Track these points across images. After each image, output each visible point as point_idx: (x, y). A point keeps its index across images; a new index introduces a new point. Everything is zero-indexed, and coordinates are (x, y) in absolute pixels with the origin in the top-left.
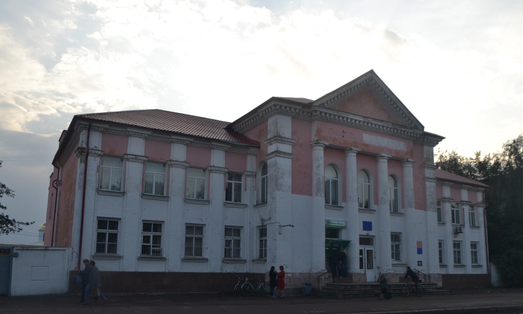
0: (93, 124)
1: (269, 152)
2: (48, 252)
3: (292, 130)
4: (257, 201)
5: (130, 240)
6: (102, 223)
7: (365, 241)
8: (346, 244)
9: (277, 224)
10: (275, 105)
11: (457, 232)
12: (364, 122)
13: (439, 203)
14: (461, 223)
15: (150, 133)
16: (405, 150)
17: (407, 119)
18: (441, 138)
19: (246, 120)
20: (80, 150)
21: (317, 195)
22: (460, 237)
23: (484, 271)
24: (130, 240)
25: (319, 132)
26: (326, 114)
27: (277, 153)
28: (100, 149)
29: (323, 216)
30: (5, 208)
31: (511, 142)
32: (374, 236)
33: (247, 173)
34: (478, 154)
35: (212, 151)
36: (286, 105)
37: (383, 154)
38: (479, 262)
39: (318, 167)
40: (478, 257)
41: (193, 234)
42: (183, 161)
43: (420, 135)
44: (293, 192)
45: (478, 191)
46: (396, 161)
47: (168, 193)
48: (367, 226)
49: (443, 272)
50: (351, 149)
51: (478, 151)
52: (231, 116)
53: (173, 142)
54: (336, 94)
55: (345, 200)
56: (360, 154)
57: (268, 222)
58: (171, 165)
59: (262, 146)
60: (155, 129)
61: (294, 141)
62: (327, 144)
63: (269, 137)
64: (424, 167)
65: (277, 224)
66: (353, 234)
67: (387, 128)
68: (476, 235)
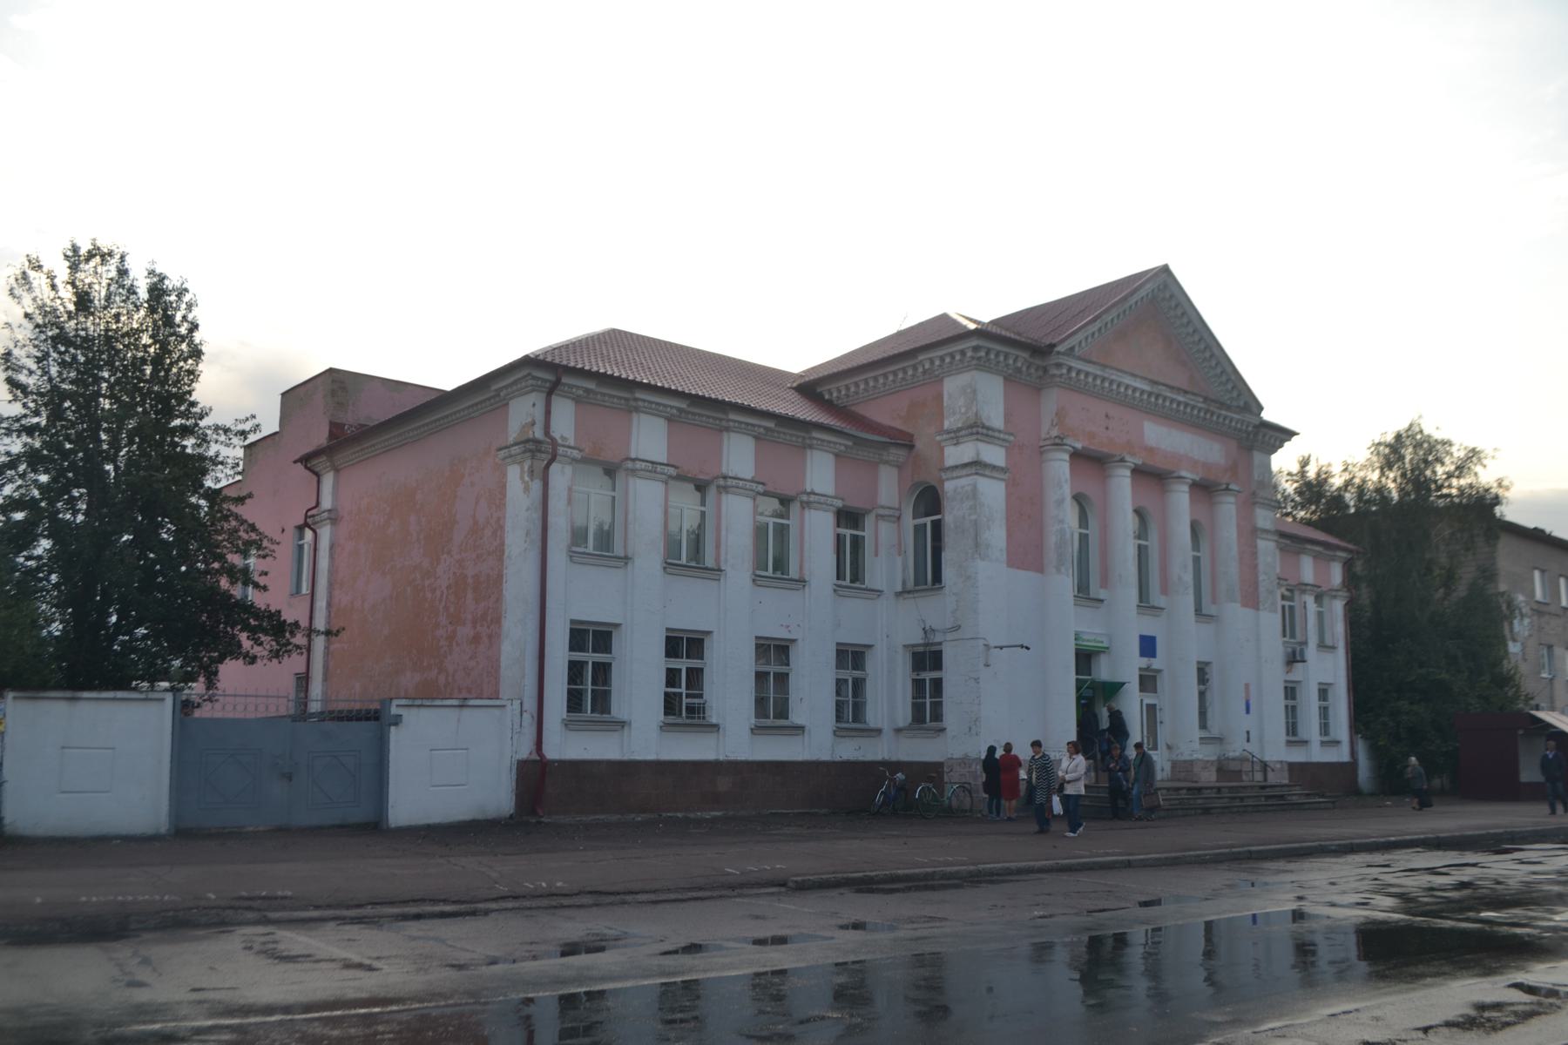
0: (564, 380)
1: (949, 462)
2: (466, 711)
3: (1006, 409)
4: (904, 583)
5: (640, 678)
6: (580, 636)
7: (1148, 681)
9: (981, 642)
10: (976, 349)
11: (1294, 658)
12: (1150, 394)
14: (1299, 638)
15: (684, 406)
17: (1229, 386)
18: (1288, 434)
19: (881, 372)
20: (531, 446)
21: (1058, 570)
22: (1298, 672)
23: (1342, 755)
24: (640, 678)
25: (1060, 414)
26: (1079, 372)
28: (572, 443)
29: (1071, 626)
30: (265, 588)
31: (1390, 438)
32: (1159, 671)
33: (881, 512)
34: (1305, 463)
35: (809, 452)
36: (998, 347)
37: (1184, 473)
38: (1333, 736)
39: (1060, 502)
40: (1331, 720)
42: (749, 477)
43: (1255, 427)
45: (1333, 559)
46: (1205, 489)
47: (717, 559)
48: (1148, 646)
49: (1297, 756)
50: (1122, 460)
52: (800, 353)
53: (727, 429)
55: (1105, 582)
56: (1137, 471)
57: (949, 636)
58: (724, 489)
59: (919, 444)
60: (697, 396)
62: (1079, 446)
63: (946, 425)
64: (1255, 503)
65: (981, 642)
66: (1124, 666)
67: (1193, 407)
68: (1329, 668)
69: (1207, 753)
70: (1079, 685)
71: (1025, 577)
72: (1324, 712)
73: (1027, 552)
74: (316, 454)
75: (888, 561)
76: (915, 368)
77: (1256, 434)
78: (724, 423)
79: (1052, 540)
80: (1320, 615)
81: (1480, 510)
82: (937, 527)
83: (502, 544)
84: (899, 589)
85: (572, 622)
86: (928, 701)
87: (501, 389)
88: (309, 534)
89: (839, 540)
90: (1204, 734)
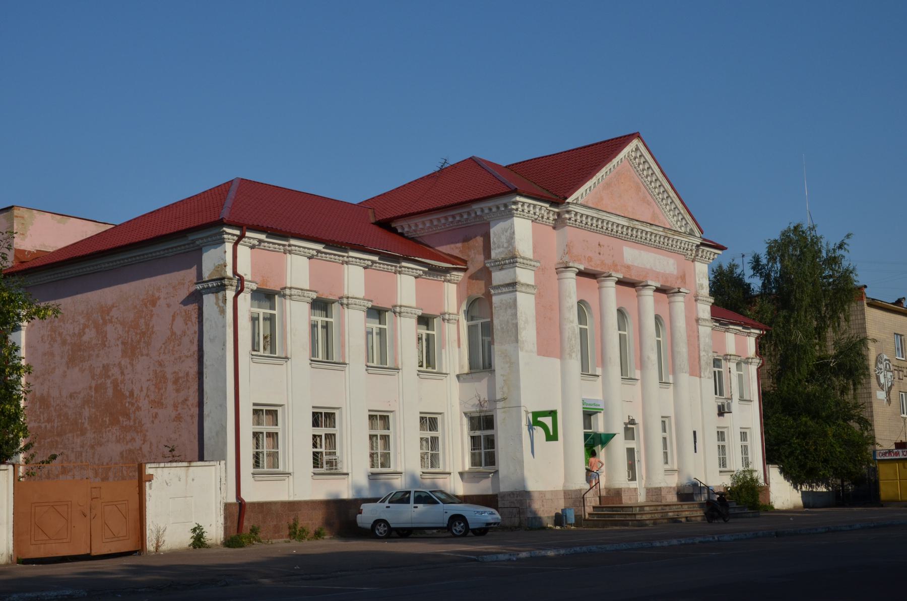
0: (248, 234)
5: (297, 437)
12: (628, 228)
13: (717, 363)
16: (675, 272)
24: (297, 437)
37: (650, 283)
41: (485, 448)
42: (361, 297)
44: (540, 353)
45: (749, 334)
61: (538, 264)
62: (582, 267)
68: (748, 416)
69: (673, 481)
70: (586, 436)
72: (745, 449)
73: (549, 346)
76: (469, 214)
77: (697, 251)
78: (345, 259)
79: (567, 334)
80: (740, 377)
85: (254, 404)
86: (483, 451)
87: (198, 239)
90: (667, 467)
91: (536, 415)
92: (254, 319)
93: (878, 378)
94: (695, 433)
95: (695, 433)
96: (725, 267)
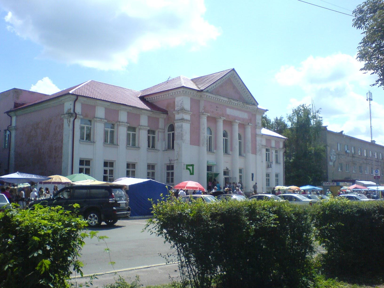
8: (217, 175)
10: (183, 91)
20: (70, 115)
22: (270, 170)
27: (182, 120)
28: (80, 113)
44: (191, 144)
46: (242, 126)
51: (275, 118)
54: (254, 102)
62: (209, 115)
71: (195, 147)
73: (195, 141)
74: (10, 111)
75: (161, 144)
79: (202, 138)
81: (320, 129)
82: (173, 134)
83: (62, 138)
84: (164, 149)
85: (80, 158)
88: (8, 133)
89: (149, 137)
91: (187, 166)
92: (82, 128)
93: (330, 158)
94: (253, 174)
95: (253, 174)
96: (279, 118)
